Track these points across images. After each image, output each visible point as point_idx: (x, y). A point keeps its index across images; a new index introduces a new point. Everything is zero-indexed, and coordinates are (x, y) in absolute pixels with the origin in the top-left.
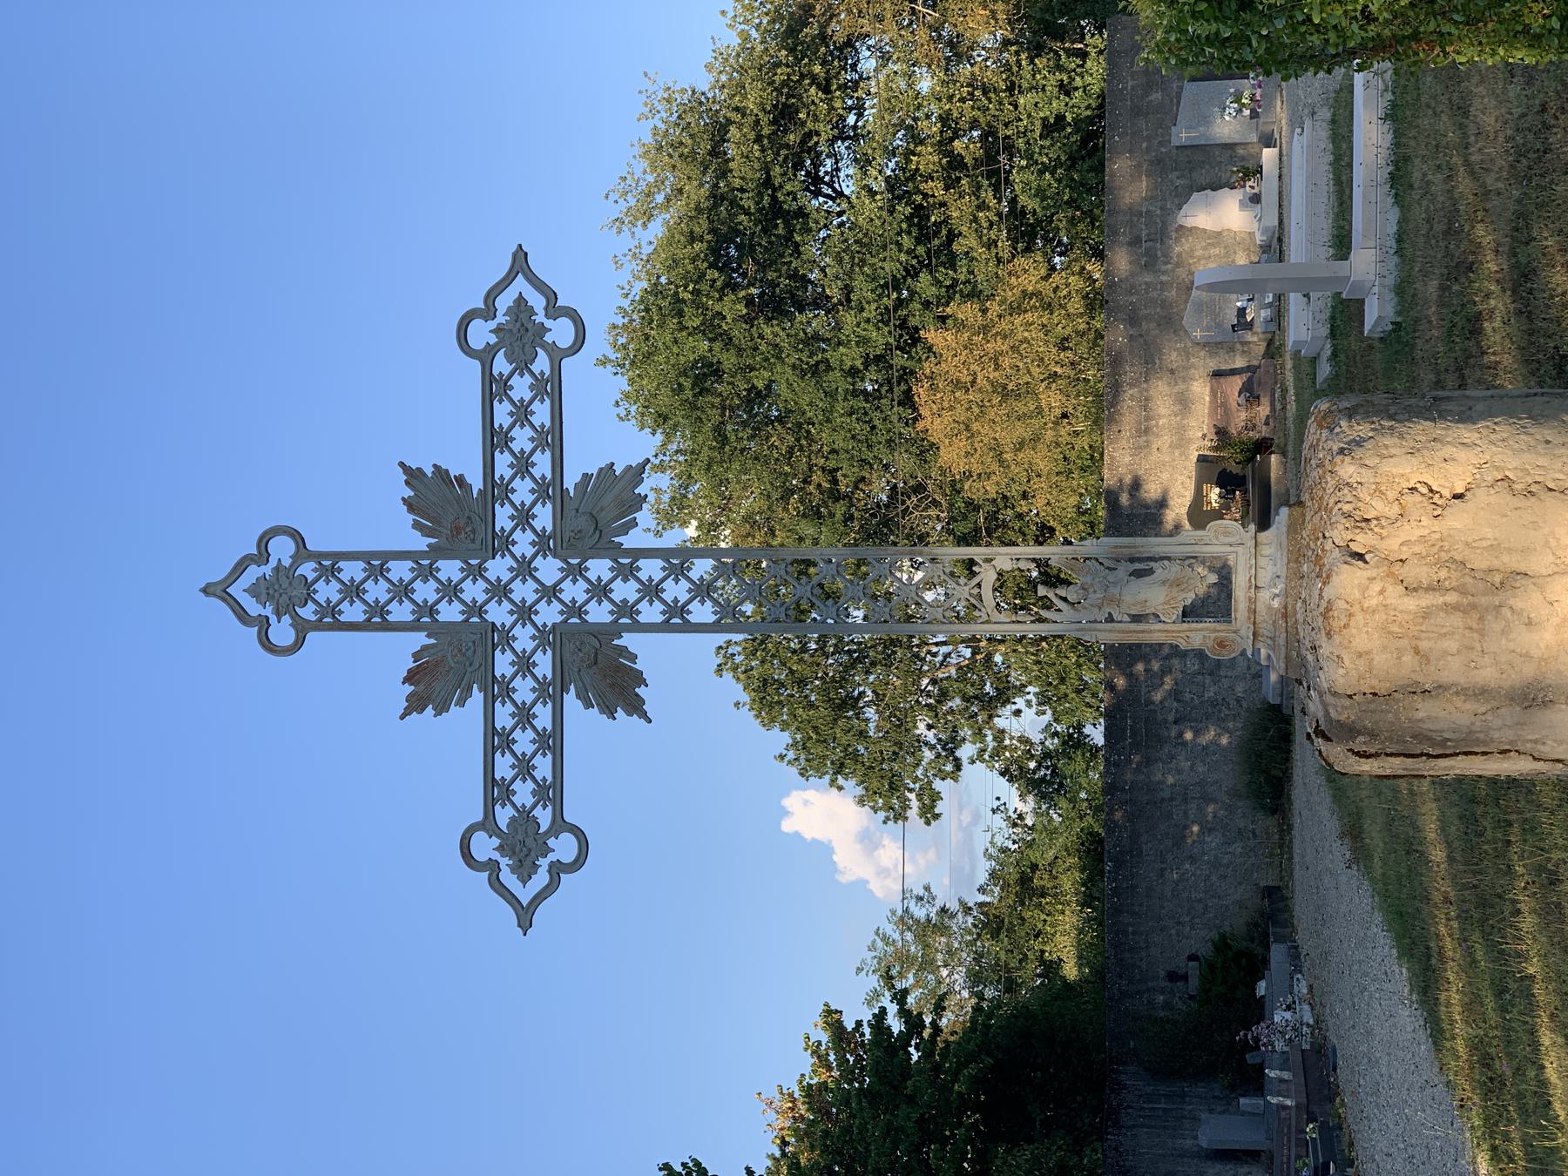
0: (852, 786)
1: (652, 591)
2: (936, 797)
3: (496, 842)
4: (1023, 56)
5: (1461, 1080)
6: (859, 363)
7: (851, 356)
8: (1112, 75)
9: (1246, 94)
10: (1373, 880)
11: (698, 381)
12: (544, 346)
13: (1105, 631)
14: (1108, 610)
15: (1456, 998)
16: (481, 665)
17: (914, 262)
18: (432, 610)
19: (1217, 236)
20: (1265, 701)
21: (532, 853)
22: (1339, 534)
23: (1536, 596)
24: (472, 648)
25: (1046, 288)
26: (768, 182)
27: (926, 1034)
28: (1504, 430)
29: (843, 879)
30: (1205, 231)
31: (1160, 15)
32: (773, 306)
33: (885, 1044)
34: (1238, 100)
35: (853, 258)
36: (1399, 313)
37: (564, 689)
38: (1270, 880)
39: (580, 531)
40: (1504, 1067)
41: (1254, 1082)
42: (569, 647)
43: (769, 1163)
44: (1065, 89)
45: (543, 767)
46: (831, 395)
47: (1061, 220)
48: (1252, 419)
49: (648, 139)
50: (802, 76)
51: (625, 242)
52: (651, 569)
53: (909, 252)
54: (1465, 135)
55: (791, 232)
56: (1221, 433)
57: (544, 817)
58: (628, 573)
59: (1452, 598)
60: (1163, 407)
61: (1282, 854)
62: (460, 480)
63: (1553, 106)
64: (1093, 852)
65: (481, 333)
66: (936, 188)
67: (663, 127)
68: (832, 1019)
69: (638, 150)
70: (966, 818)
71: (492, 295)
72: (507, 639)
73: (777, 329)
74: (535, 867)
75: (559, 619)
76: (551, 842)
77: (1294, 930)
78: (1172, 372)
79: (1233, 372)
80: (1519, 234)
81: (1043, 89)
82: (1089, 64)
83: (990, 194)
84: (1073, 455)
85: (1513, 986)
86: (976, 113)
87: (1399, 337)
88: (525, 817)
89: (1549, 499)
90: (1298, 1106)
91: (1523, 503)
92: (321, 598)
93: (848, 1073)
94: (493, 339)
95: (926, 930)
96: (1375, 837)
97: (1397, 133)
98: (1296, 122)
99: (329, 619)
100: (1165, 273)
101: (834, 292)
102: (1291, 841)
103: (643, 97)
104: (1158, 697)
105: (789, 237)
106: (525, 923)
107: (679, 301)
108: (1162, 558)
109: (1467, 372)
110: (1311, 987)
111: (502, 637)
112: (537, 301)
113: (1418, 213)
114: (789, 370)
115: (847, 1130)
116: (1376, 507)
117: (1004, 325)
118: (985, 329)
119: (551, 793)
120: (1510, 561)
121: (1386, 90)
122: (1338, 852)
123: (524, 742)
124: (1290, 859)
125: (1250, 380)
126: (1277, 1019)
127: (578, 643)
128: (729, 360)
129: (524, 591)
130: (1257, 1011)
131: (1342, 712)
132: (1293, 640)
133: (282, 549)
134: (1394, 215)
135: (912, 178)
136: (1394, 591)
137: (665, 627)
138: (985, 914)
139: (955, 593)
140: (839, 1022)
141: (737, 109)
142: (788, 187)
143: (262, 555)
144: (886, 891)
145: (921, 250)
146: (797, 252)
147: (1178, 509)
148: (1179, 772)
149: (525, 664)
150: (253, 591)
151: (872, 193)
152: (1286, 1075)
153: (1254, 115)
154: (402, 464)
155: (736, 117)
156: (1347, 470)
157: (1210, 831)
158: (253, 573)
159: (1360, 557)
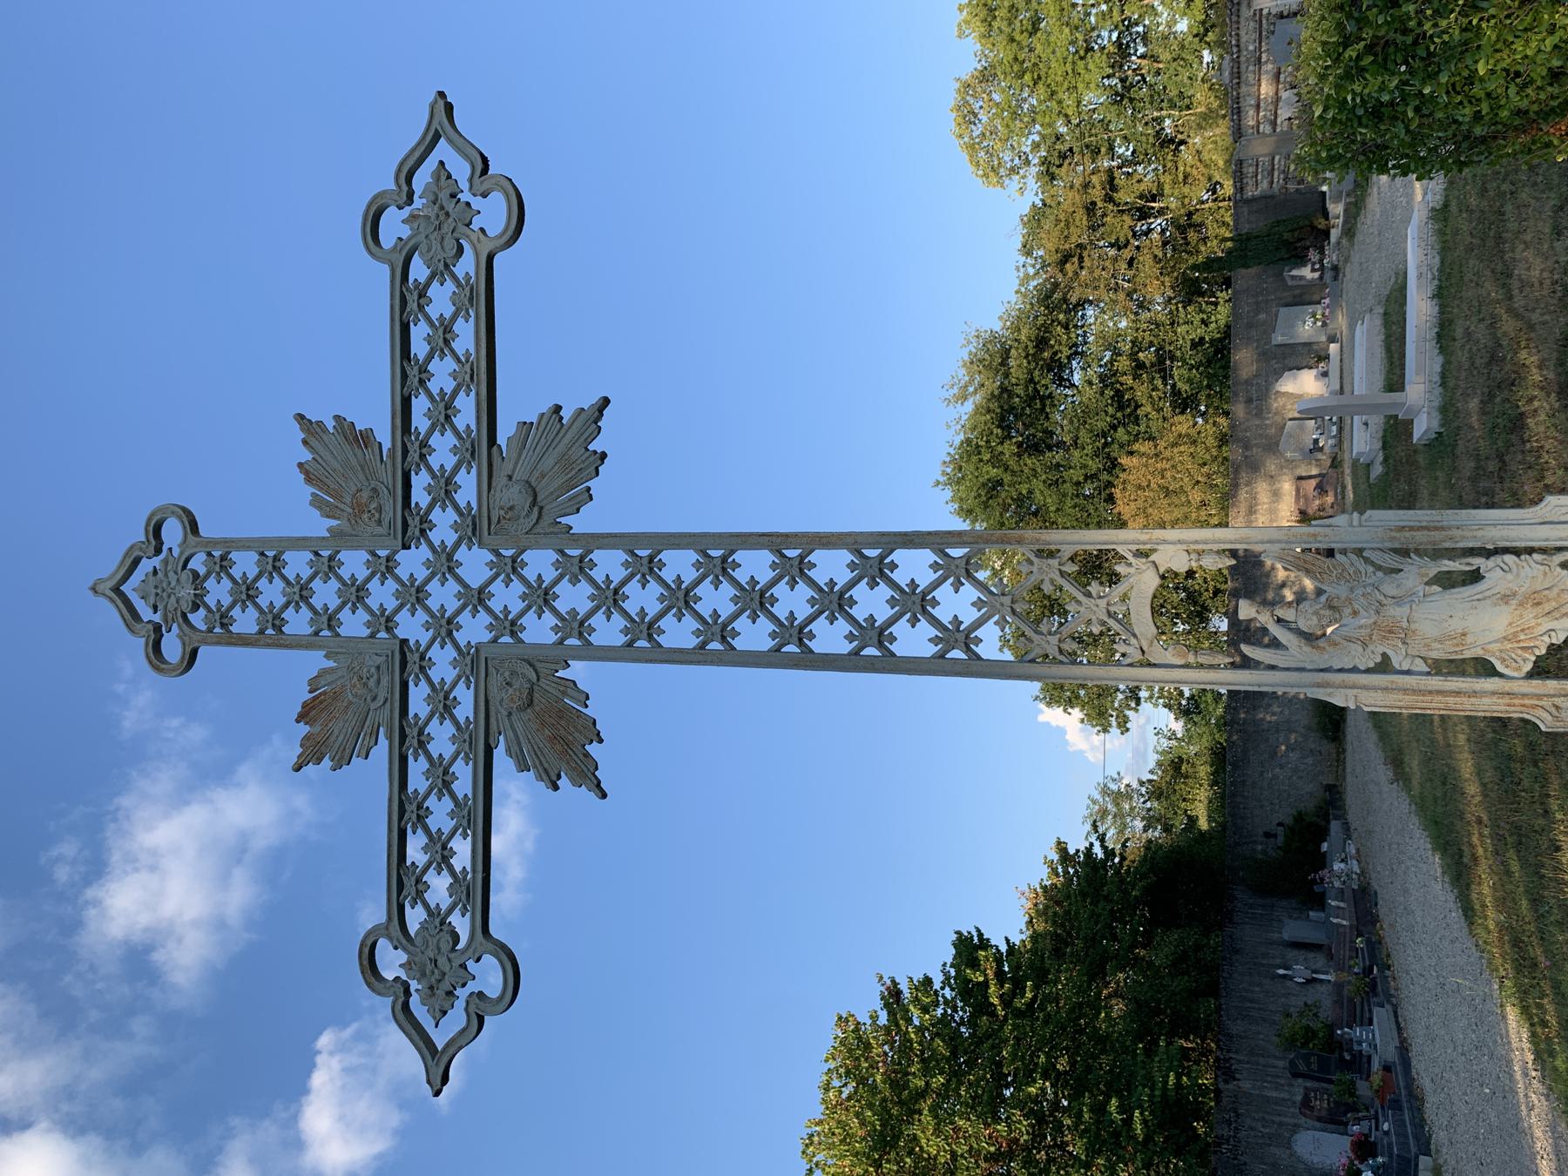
1: (610, 598)
2: (1126, 720)
4: (1180, 305)
7: (1077, 475)
8: (1234, 312)
9: (1319, 312)
13: (1375, 689)
14: (1381, 649)
16: (387, 699)
17: (1115, 422)
21: (446, 977)
24: (375, 677)
25: (1193, 432)
26: (1031, 380)
30: (1292, 394)
32: (1033, 447)
34: (1314, 316)
35: (1079, 421)
36: (1442, 426)
39: (511, 508)
42: (496, 681)
44: (1205, 323)
46: (1065, 495)
49: (966, 358)
50: (1053, 321)
53: (1111, 416)
55: (1044, 406)
57: (461, 924)
58: (579, 569)
60: (1263, 496)
61: (1338, 766)
64: (1220, 757)
66: (1128, 379)
67: (974, 350)
68: (1062, 848)
69: (961, 363)
73: (1035, 461)
77: (1345, 812)
78: (1272, 477)
79: (1310, 477)
81: (1192, 323)
82: (1219, 308)
83: (1160, 382)
86: (1152, 338)
87: (1440, 444)
90: (1351, 926)
96: (1414, 764)
97: (1443, 310)
100: (1268, 418)
101: (1067, 439)
102: (1345, 758)
103: (964, 335)
105: (1043, 409)
107: (978, 446)
108: (1498, 551)
109: (1507, 458)
110: (1358, 851)
113: (1462, 357)
114: (1041, 484)
115: (1067, 913)
117: (1167, 454)
118: (1157, 455)
121: (1434, 279)
124: (1344, 770)
125: (1321, 482)
126: (1335, 868)
127: (507, 674)
128: (1007, 478)
129: (443, 595)
130: (1321, 862)
133: (173, 533)
134: (1440, 360)
135: (1114, 375)
138: (1153, 786)
139: (1082, 609)
140: (1066, 849)
141: (1016, 340)
142: (1043, 382)
145: (1119, 415)
146: (1047, 418)
151: (1090, 383)
152: (1342, 905)
153: (1324, 324)
154: (300, 417)
157: (1293, 750)
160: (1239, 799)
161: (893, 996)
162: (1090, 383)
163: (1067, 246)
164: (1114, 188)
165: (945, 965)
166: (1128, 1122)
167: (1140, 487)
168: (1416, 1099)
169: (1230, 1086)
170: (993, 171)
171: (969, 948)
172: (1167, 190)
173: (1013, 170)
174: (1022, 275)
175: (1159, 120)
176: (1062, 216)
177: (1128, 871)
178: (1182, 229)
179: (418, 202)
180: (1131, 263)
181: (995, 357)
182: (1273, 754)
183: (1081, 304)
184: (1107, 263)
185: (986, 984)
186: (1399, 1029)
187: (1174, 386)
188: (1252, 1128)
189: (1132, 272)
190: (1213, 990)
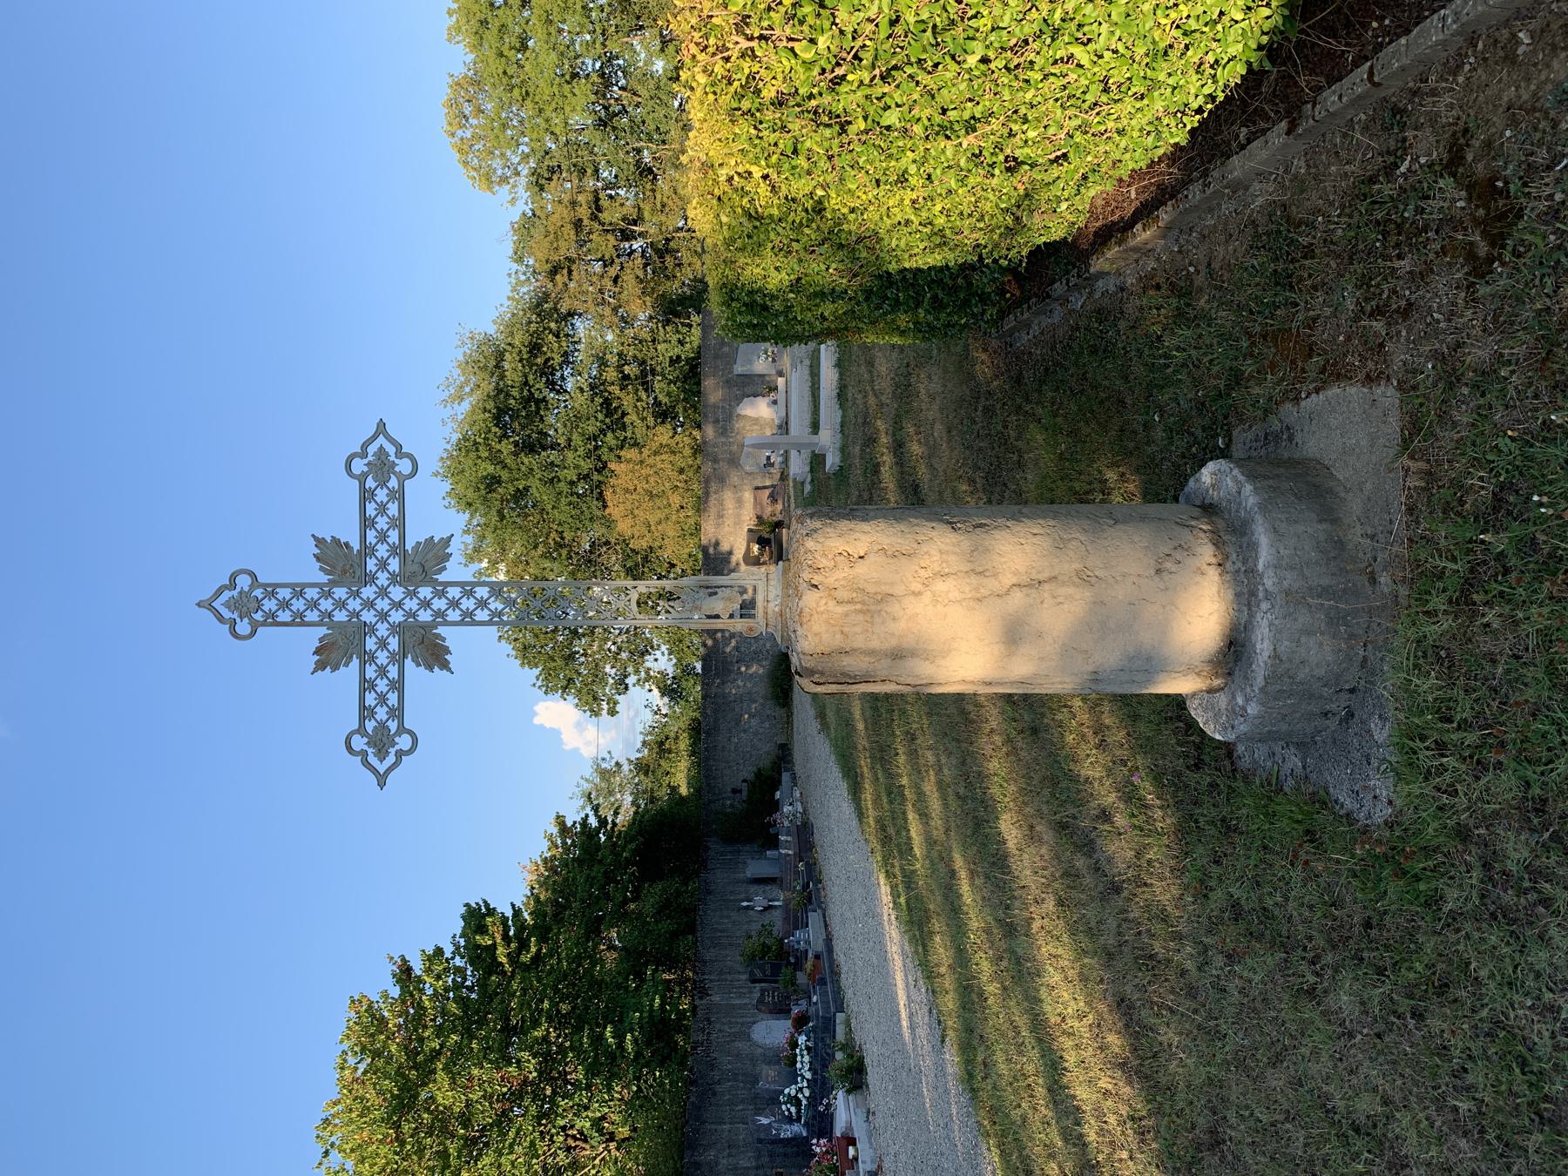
0: (572, 700)
1: (454, 604)
3: (365, 740)
5: (871, 838)
6: (575, 478)
7: (571, 475)
8: (704, 337)
10: (831, 740)
11: (488, 486)
12: (395, 473)
15: (869, 797)
18: (330, 615)
19: (756, 420)
20: (780, 651)
22: (806, 575)
23: (897, 606)
25: (672, 442)
26: (526, 383)
27: (609, 827)
28: (882, 525)
29: (567, 748)
31: (722, 312)
32: (529, 447)
33: (587, 833)
34: (766, 353)
37: (405, 657)
38: (781, 740)
40: (891, 831)
41: (774, 843)
42: (408, 634)
43: (525, 899)
44: (681, 343)
45: (393, 699)
47: (679, 408)
48: (773, 511)
49: (461, 358)
51: (448, 412)
52: (454, 592)
54: (872, 376)
55: (538, 408)
56: (759, 517)
57: (393, 726)
58: (441, 594)
59: (858, 606)
62: (347, 544)
63: (913, 364)
64: (696, 729)
65: (359, 466)
66: (615, 389)
68: (560, 820)
70: (632, 713)
71: (365, 446)
72: (373, 630)
74: (388, 753)
75: (403, 619)
76: (397, 739)
79: (765, 487)
80: (897, 425)
84: (686, 528)
85: (895, 790)
87: (842, 473)
88: (382, 726)
89: (903, 559)
91: (891, 561)
92: (266, 608)
93: (566, 849)
94: (366, 469)
95: (605, 774)
97: (841, 374)
98: (794, 365)
99: (271, 620)
101: (562, 441)
104: (728, 650)
105: (537, 412)
106: (382, 784)
107: (475, 443)
111: (367, 629)
112: (391, 449)
113: (851, 413)
115: (566, 880)
116: (823, 562)
117: (650, 461)
118: (642, 462)
119: (397, 713)
120: (885, 589)
122: (814, 726)
123: (382, 686)
128: (505, 475)
129: (383, 604)
130: (775, 806)
131: (808, 663)
132: (785, 626)
133: (244, 582)
134: (839, 413)
135: (603, 384)
136: (832, 603)
137: (461, 623)
140: (564, 822)
142: (537, 386)
143: (232, 584)
144: (588, 752)
145: (608, 420)
146: (542, 420)
147: (738, 555)
148: (739, 687)
149: (383, 644)
150: (227, 605)
151: (582, 390)
152: (789, 839)
153: (774, 361)
155: (509, 348)
156: (810, 544)
158: (227, 595)
159: (816, 586)
160: (712, 763)
161: (405, 974)
162: (582, 390)
163: (557, 258)
164: (599, 209)
165: (454, 936)
166: (621, 1045)
167: (627, 491)
168: (835, 973)
169: (704, 1002)
170: (489, 180)
171: (477, 918)
172: (646, 215)
173: (504, 180)
174: (514, 281)
175: (639, 151)
176: (551, 229)
177: (619, 837)
178: (661, 253)
179: (370, 458)
180: (615, 280)
181: (492, 359)
182: (738, 721)
183: (571, 314)
184: (594, 279)
185: (494, 946)
186: (826, 926)
187: (655, 398)
188: (720, 1031)
189: (617, 290)
190: (691, 928)
